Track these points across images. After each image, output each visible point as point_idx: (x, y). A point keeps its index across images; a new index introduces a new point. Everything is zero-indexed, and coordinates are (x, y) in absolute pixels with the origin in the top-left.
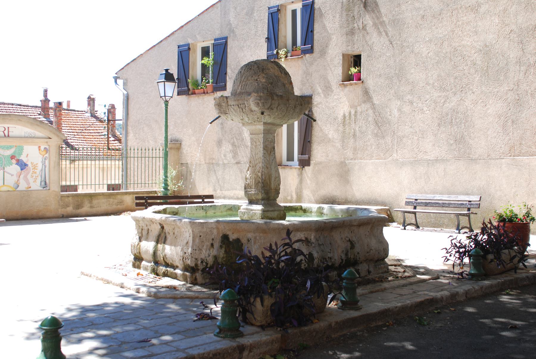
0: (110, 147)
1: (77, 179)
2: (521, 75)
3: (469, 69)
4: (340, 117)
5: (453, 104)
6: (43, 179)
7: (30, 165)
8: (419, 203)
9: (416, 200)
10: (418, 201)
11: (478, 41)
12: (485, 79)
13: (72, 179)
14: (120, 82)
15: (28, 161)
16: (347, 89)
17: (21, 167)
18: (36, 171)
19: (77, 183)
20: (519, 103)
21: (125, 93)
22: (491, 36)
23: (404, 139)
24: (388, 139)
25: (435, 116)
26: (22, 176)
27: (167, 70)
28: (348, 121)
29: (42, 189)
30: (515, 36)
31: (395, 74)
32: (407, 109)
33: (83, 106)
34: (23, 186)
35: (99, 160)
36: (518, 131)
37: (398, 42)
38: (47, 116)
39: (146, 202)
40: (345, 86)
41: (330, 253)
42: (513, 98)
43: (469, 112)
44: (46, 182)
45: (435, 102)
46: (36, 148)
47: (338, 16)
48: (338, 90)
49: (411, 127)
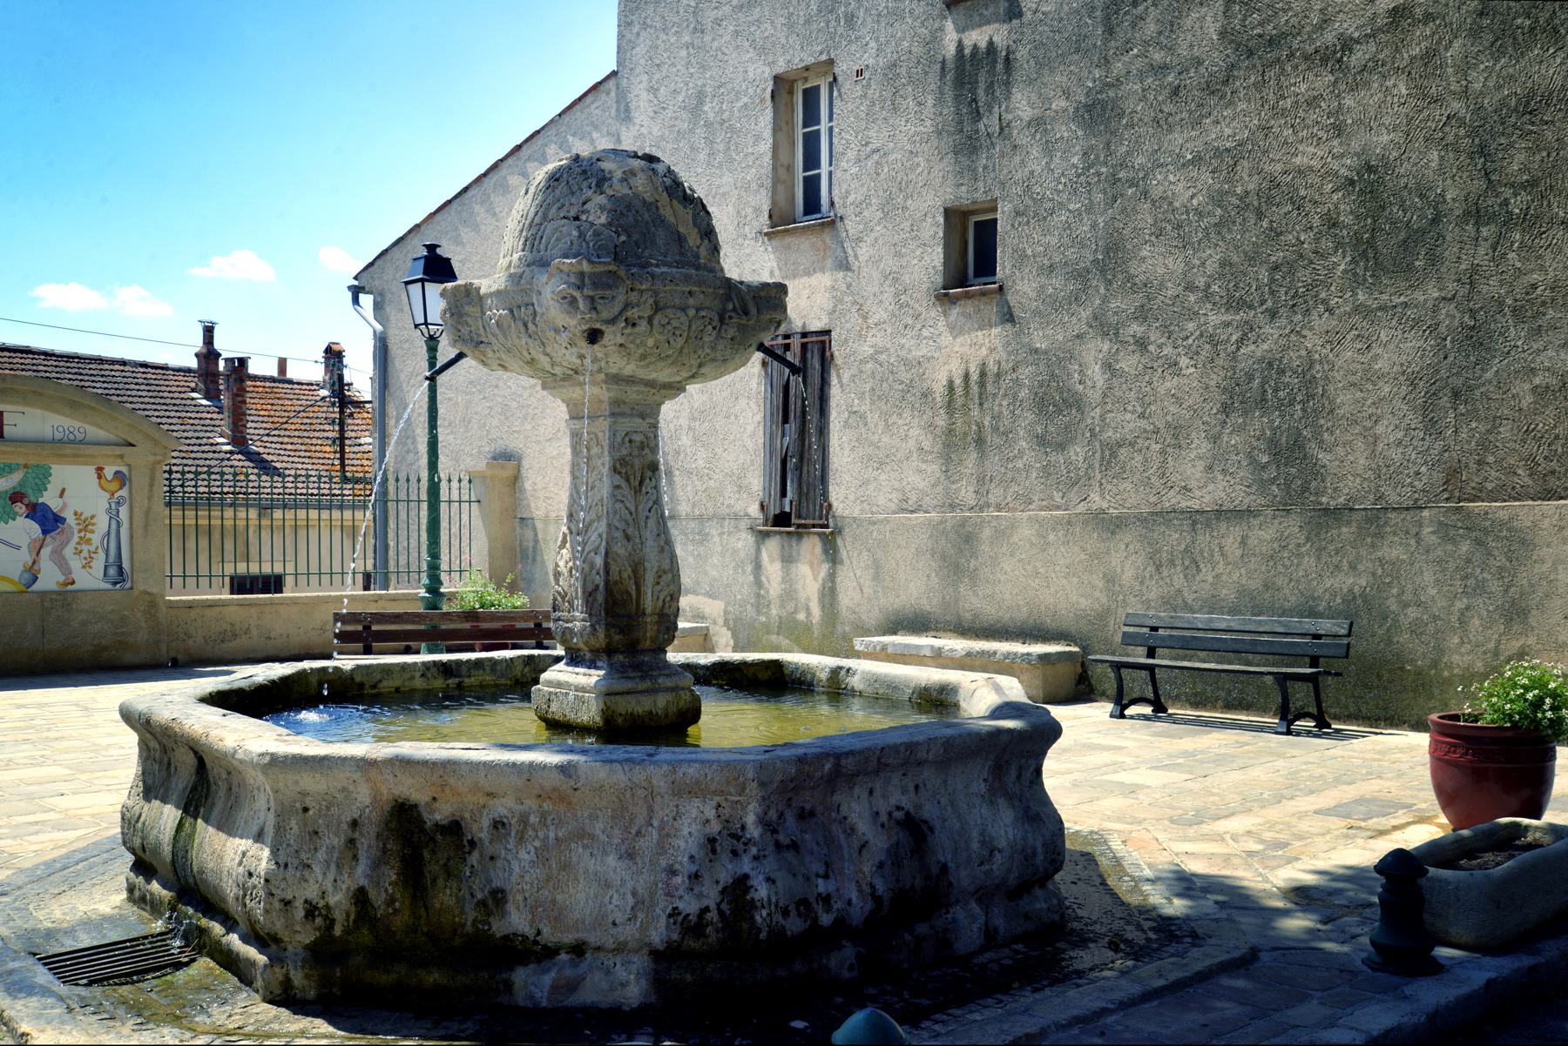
0: (349, 475)
1: (278, 555)
2: (1481, 251)
3: (1317, 240)
4: (939, 388)
5: (1265, 347)
6: (111, 560)
7: (69, 516)
8: (1163, 638)
9: (1154, 629)
10: (1161, 632)
11: (1342, 156)
12: (1366, 269)
13: (266, 556)
14: (366, 300)
15: (63, 509)
16: (955, 311)
17: (42, 524)
18: (89, 535)
19: (278, 569)
20: (1476, 338)
21: (379, 327)
22: (1385, 138)
23: (1123, 450)
24: (1077, 452)
25: (1213, 383)
26: (46, 552)
27: (432, 248)
28: (959, 401)
29: (109, 586)
30: (1462, 132)
31: (1096, 261)
32: (1129, 363)
33: (317, 373)
34: (49, 579)
35: (247, 506)
36: (1474, 425)
37: (1104, 170)
38: (212, 395)
39: (367, 628)
40: (953, 300)
41: (826, 877)
42: (1456, 323)
43: (1318, 367)
44: (120, 568)
45: (1214, 341)
46: (91, 471)
47: (930, 102)
48: (933, 313)
49: (1142, 416)
